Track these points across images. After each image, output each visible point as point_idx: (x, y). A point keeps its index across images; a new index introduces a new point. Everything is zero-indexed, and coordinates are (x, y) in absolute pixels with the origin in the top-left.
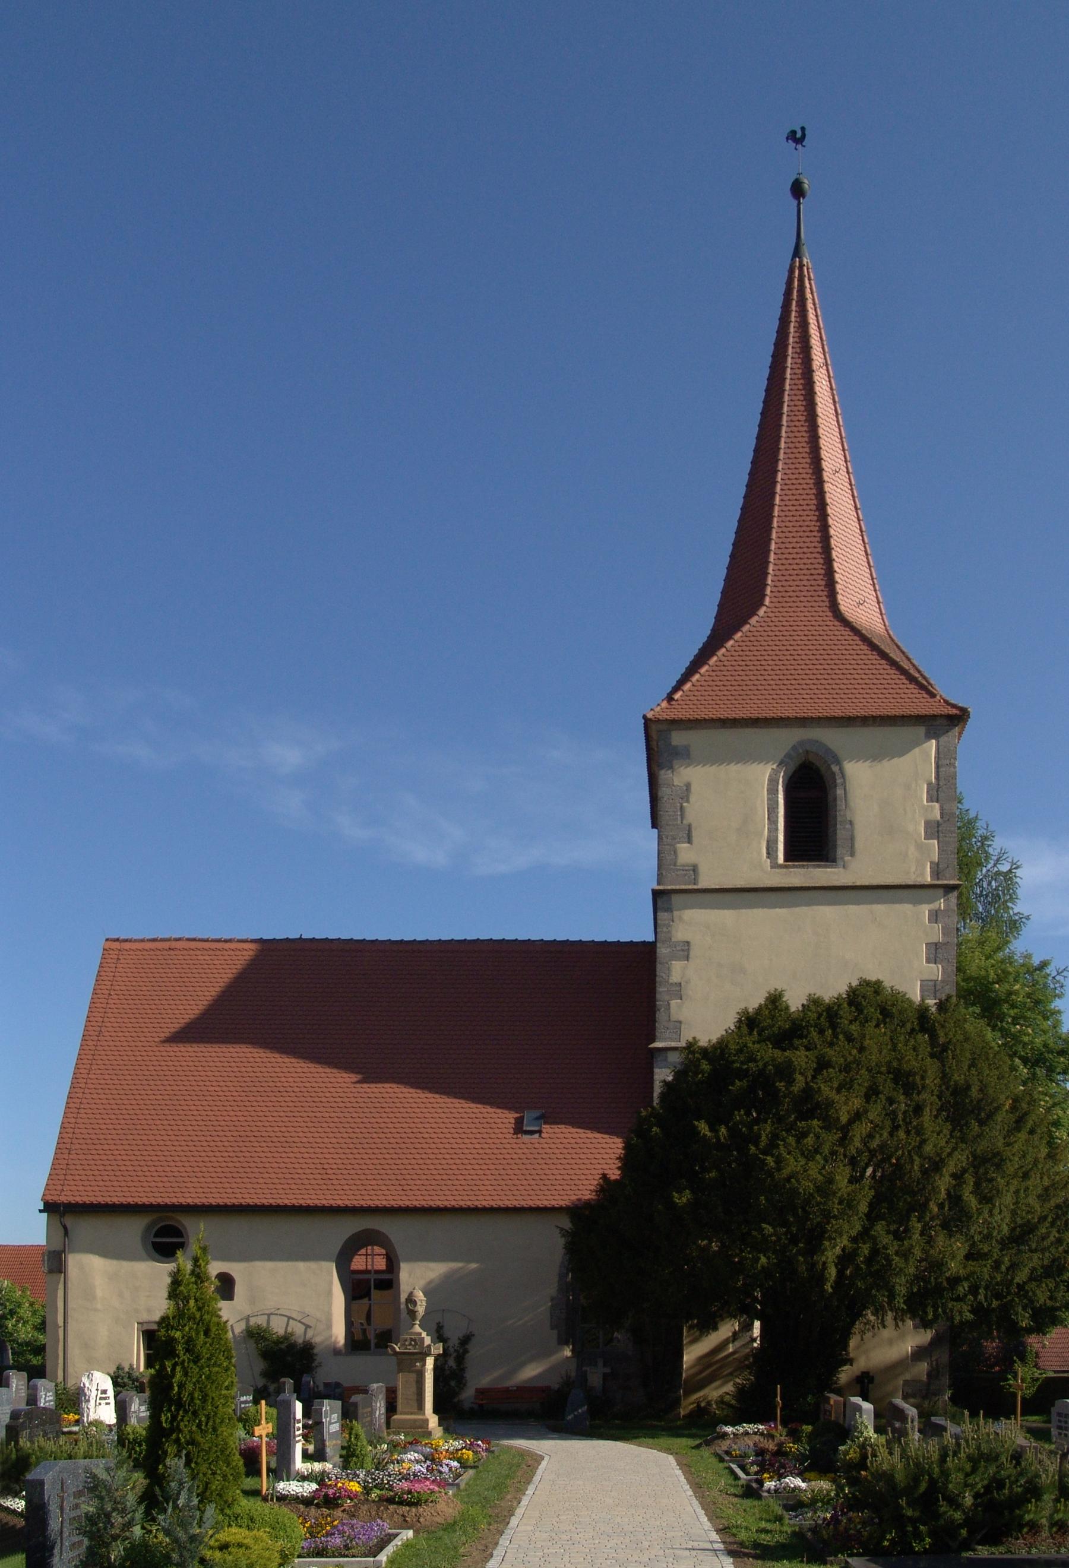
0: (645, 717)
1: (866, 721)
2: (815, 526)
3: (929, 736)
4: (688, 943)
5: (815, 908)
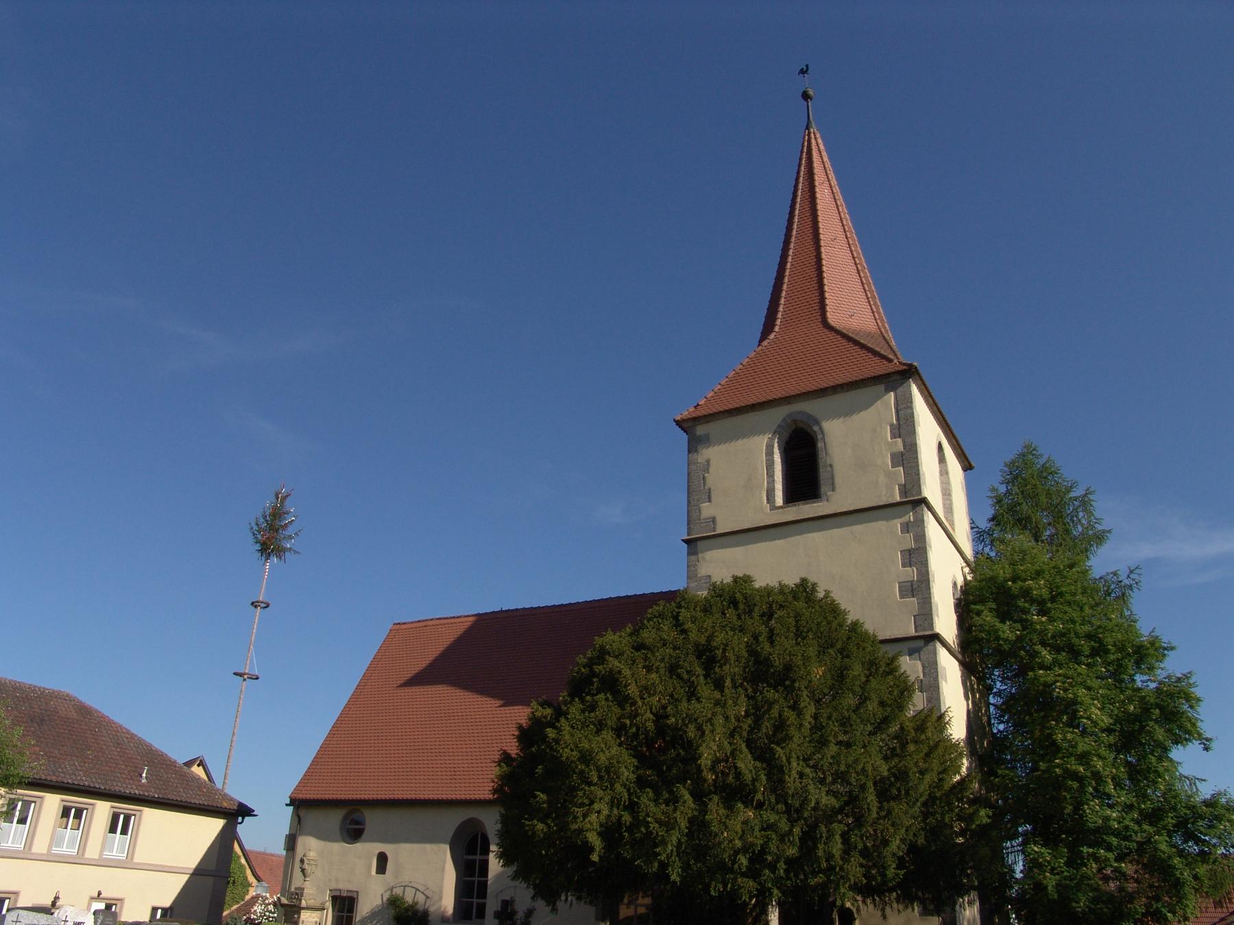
0: (678, 423)
2: (814, 275)
3: (887, 390)
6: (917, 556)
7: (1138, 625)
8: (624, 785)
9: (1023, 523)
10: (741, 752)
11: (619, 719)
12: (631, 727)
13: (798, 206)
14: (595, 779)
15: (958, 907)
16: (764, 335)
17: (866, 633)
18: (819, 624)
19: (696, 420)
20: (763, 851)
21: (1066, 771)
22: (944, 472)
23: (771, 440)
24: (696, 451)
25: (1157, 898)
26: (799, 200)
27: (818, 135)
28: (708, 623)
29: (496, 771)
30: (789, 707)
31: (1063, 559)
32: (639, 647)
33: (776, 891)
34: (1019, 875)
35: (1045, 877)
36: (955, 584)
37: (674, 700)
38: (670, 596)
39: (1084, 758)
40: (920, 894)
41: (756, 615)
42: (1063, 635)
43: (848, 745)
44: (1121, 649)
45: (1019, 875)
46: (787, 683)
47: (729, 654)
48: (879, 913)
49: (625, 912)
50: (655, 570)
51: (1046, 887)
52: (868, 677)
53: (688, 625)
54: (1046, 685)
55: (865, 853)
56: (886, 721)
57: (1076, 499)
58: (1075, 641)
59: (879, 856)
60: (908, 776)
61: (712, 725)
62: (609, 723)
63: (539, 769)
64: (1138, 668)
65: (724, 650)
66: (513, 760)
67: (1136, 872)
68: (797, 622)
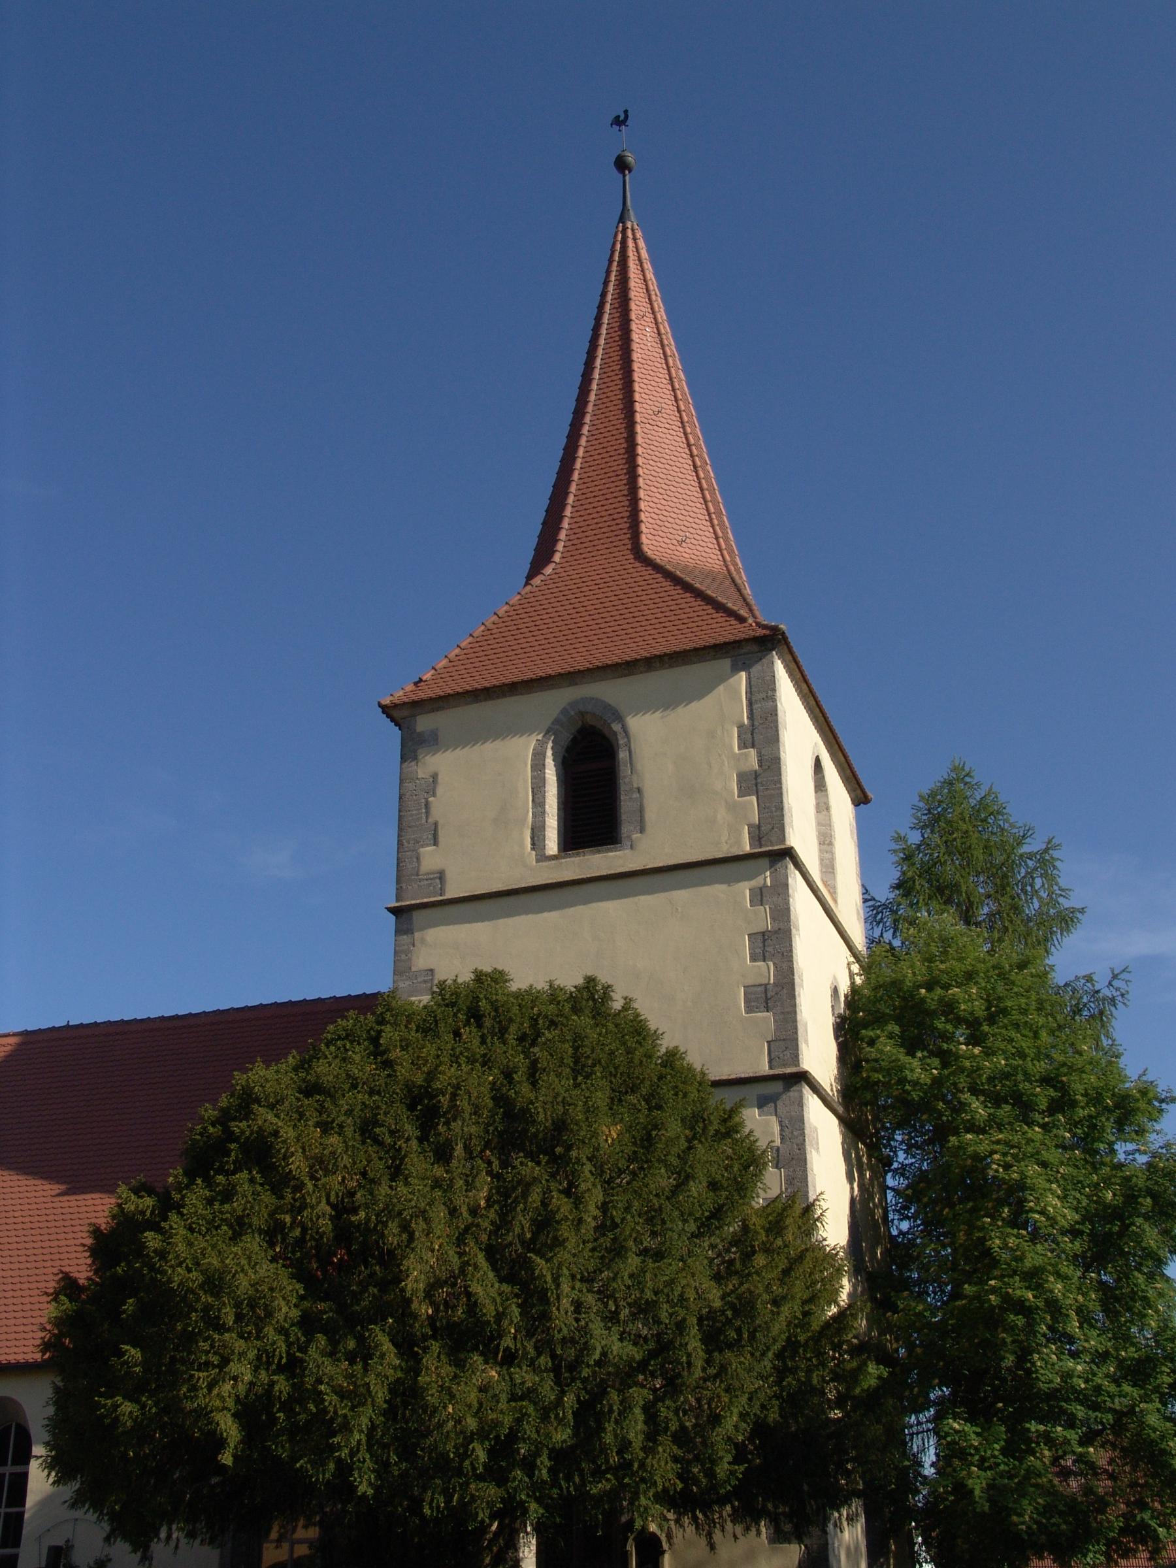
0: (385, 709)
1: (650, 663)
3: (736, 669)
4: (432, 970)
5: (594, 905)
6: (775, 943)
7: (1122, 1062)
8: (282, 1331)
9: (945, 892)
10: (476, 1267)
11: (272, 1215)
12: (292, 1228)
13: (600, 352)
14: (230, 1320)
15: (831, 1526)
16: (536, 567)
17: (690, 1068)
18: (612, 1053)
19: (417, 706)
20: (513, 1436)
21: (1006, 1298)
22: (823, 807)
23: (541, 744)
24: (415, 758)
25: (1142, 1505)
26: (602, 341)
27: (639, 234)
28: (429, 1050)
29: (50, 1310)
30: (560, 1191)
31: (1011, 951)
32: (310, 1090)
33: (533, 1506)
34: (929, 1471)
35: (970, 1474)
36: (835, 991)
37: (368, 1181)
38: (365, 1002)
39: (1034, 1278)
40: (770, 1506)
41: (511, 1038)
42: (1006, 1076)
43: (659, 1255)
44: (1095, 1099)
45: (929, 1471)
46: (559, 1150)
47: (463, 1103)
48: (703, 1541)
49: (272, 1554)
50: (341, 960)
51: (972, 1491)
52: (689, 1140)
53: (396, 1054)
54: (976, 1157)
55: (681, 1438)
56: (717, 1213)
57: (1030, 856)
58: (1025, 1086)
59: (704, 1443)
60: (753, 1307)
61: (427, 1221)
62: (255, 1221)
63: (130, 1306)
64: (1121, 1130)
65: (454, 1096)
66: (82, 1289)
67: (1111, 1461)
68: (576, 1049)
